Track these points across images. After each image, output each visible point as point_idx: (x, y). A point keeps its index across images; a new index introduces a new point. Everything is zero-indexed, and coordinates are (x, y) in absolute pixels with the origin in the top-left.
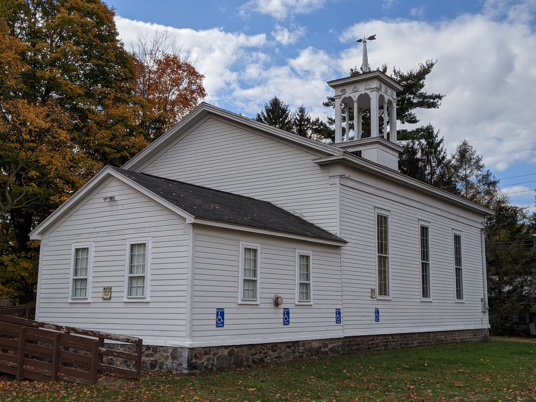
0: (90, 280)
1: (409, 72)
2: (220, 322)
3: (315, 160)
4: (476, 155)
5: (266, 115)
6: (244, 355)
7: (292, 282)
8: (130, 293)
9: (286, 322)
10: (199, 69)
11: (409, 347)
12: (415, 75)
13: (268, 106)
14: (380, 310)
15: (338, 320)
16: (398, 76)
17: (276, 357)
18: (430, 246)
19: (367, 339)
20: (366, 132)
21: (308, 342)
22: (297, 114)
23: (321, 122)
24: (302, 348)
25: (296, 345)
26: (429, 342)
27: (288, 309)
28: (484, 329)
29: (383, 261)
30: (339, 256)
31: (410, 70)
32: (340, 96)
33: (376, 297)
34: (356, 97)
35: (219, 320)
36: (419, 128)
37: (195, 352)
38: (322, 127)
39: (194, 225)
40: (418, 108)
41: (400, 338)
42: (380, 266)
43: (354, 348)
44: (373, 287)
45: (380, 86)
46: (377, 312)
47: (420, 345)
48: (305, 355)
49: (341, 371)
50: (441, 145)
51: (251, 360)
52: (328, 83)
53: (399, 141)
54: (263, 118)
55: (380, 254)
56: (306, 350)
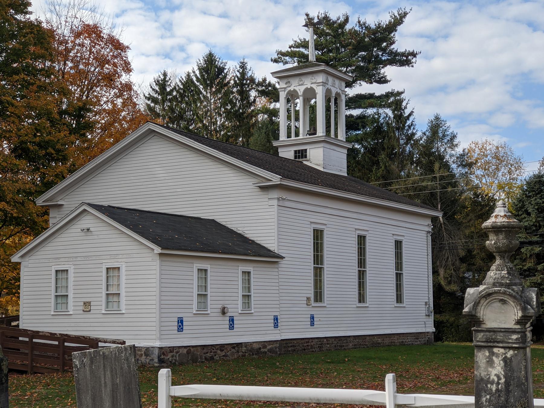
1: (377, 24)
2: (180, 328)
3: (255, 184)
4: (451, 131)
5: (198, 75)
6: (199, 353)
8: (107, 306)
9: (231, 327)
10: (124, 40)
11: (344, 349)
12: (384, 26)
13: (201, 64)
15: (276, 326)
16: (364, 28)
17: (224, 356)
19: (303, 341)
20: (313, 131)
21: (249, 344)
22: (236, 70)
23: (269, 83)
24: (245, 348)
25: (239, 346)
26: (365, 345)
27: (233, 317)
28: (428, 333)
29: (318, 272)
30: (277, 270)
31: (378, 21)
32: (285, 88)
33: (311, 304)
34: (302, 91)
36: (389, 92)
37: (163, 350)
38: (270, 88)
39: (161, 255)
40: (388, 66)
41: (335, 340)
43: (290, 349)
44: (308, 296)
45: (327, 80)
46: (312, 317)
47: (355, 347)
48: (247, 354)
49: (275, 364)
50: (411, 118)
51: (204, 358)
52: (272, 73)
53: (364, 110)
54: (194, 79)
55: (316, 266)
56: (248, 350)
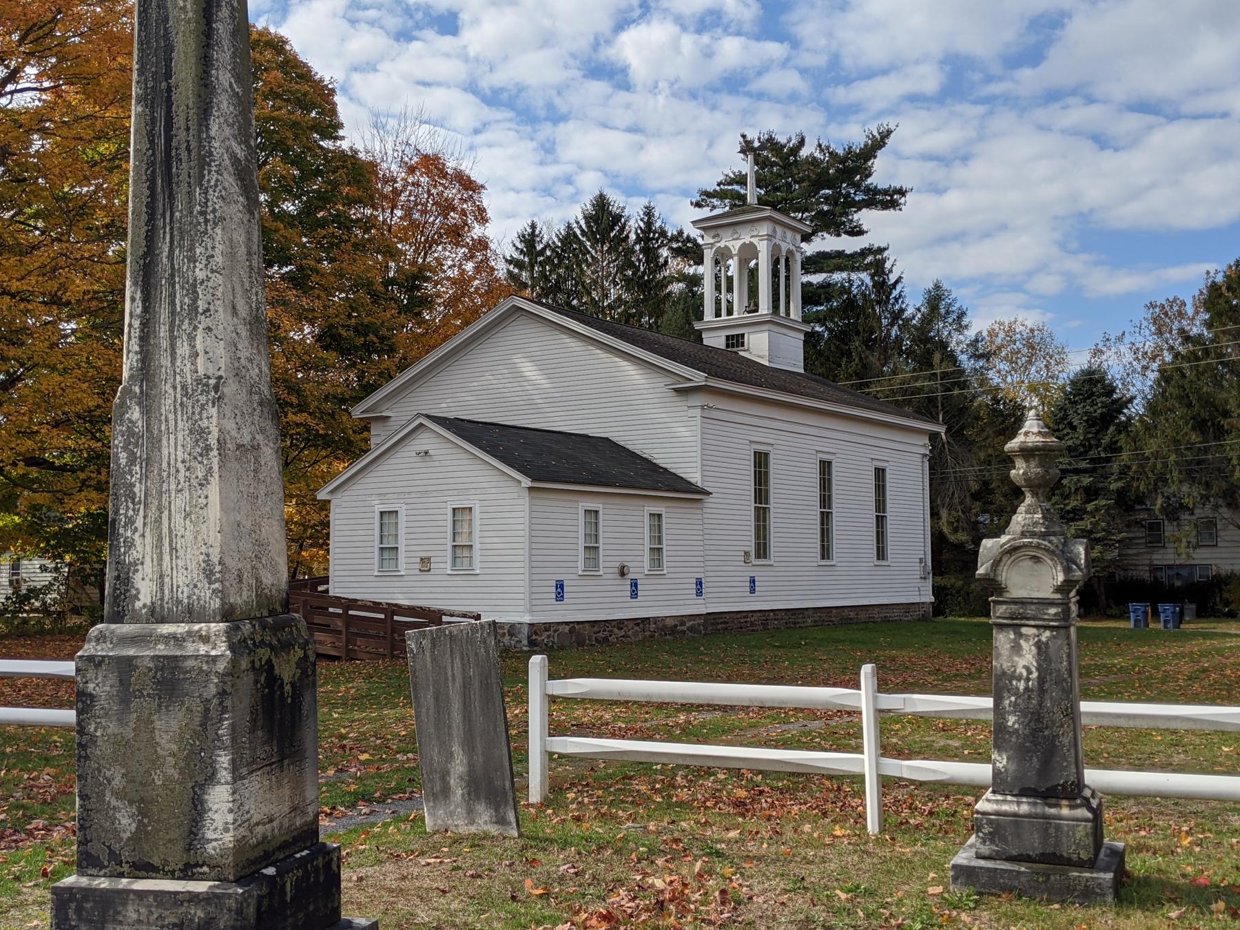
0: (402, 549)
2: (560, 596)
4: (957, 305)
5: (584, 226)
7: (641, 547)
8: (454, 564)
9: (634, 594)
14: (756, 579)
15: (699, 593)
18: (834, 487)
19: (739, 616)
20: (753, 307)
23: (688, 236)
28: (923, 603)
34: (737, 248)
35: (559, 593)
39: (530, 488)
42: (757, 519)
43: (719, 627)
44: (747, 549)
46: (753, 581)
47: (815, 624)
50: (899, 287)
54: (578, 232)
